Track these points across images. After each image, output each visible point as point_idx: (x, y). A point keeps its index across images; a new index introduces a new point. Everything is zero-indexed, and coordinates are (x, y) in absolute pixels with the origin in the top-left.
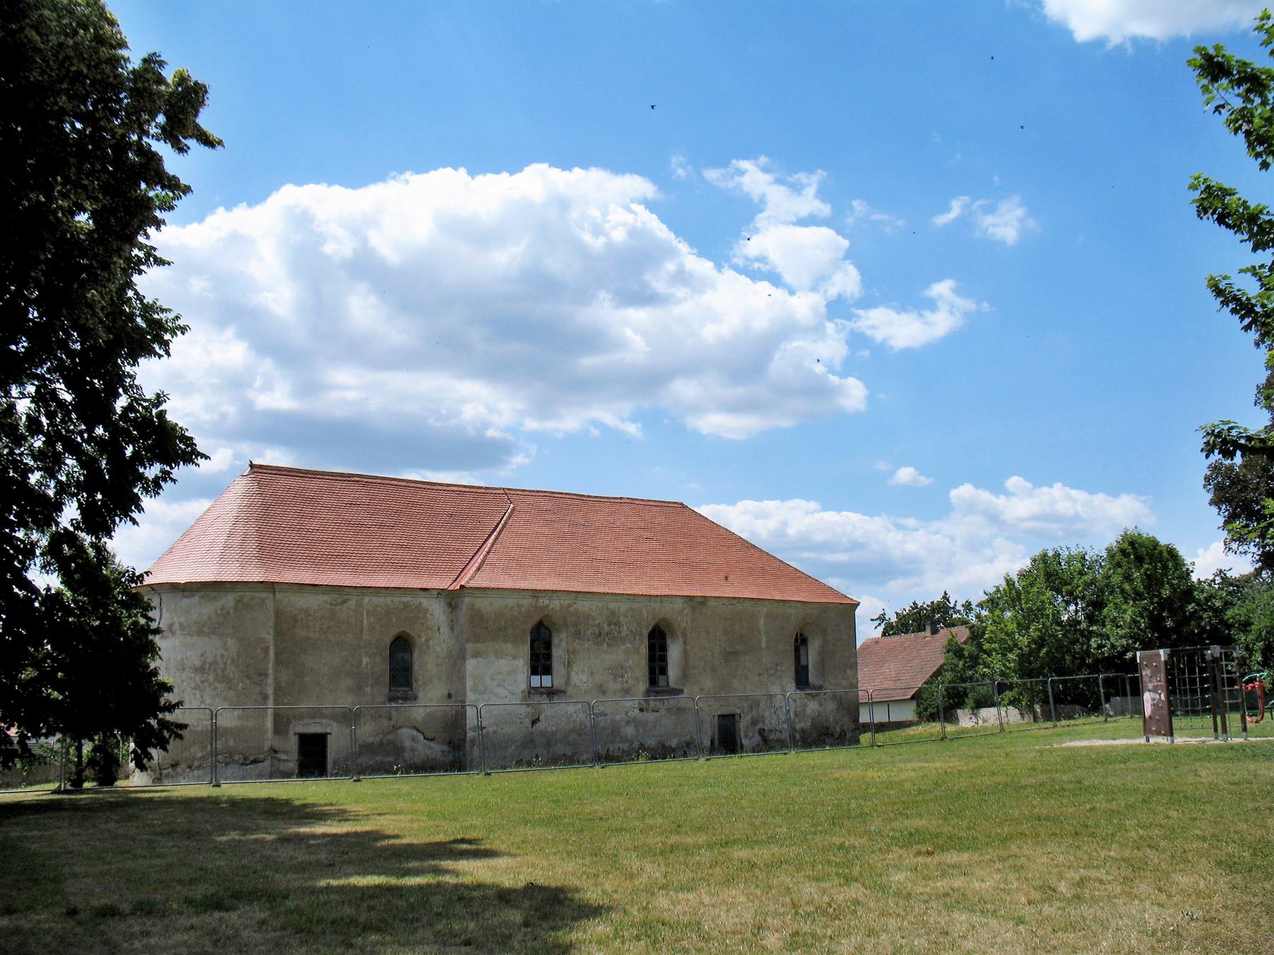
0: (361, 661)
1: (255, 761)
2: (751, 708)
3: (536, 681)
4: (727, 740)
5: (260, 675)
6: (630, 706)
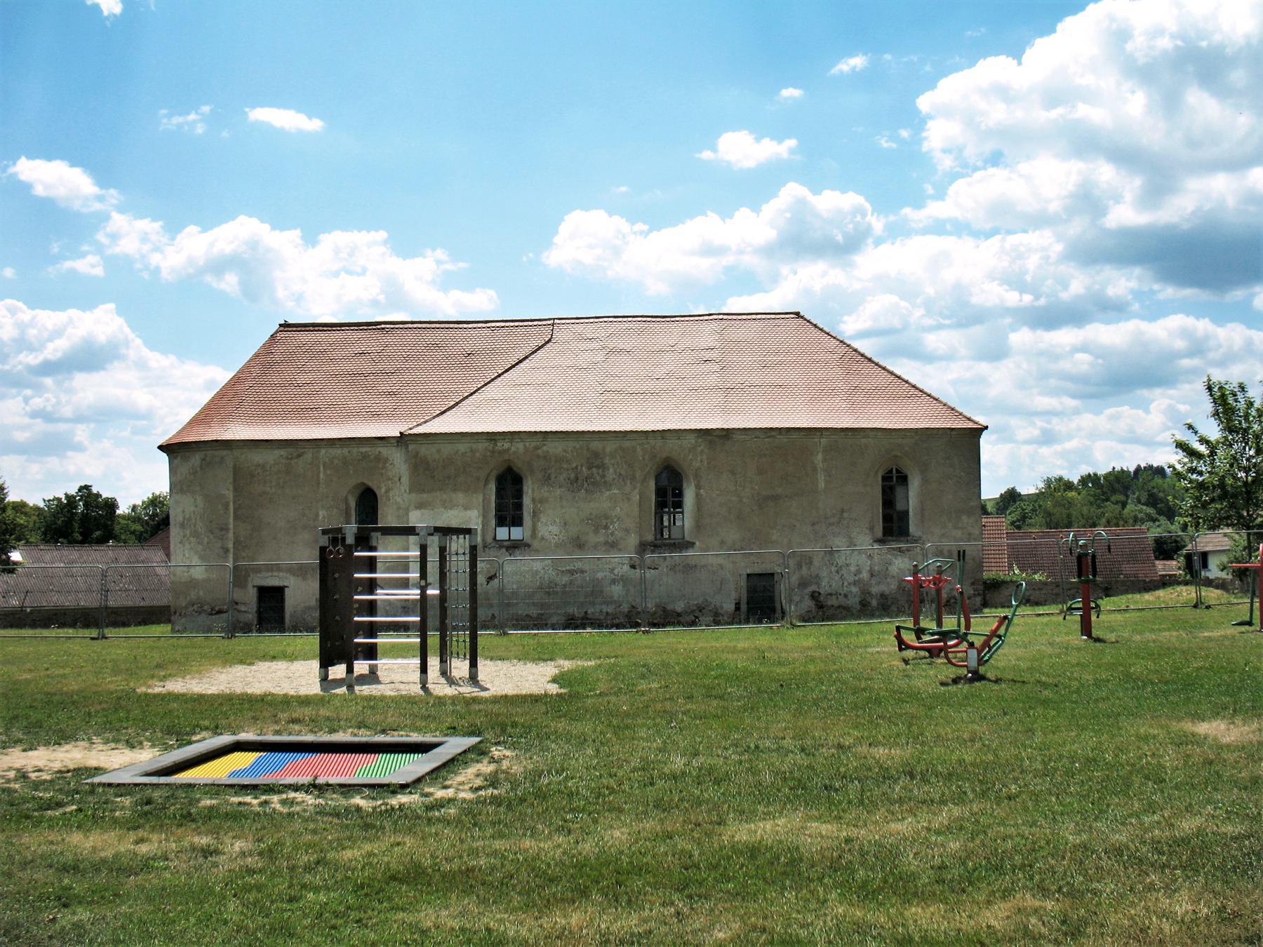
0: (317, 515)
1: (220, 612)
2: (799, 566)
3: (502, 533)
4: (760, 603)
5: (222, 529)
6: (619, 562)
